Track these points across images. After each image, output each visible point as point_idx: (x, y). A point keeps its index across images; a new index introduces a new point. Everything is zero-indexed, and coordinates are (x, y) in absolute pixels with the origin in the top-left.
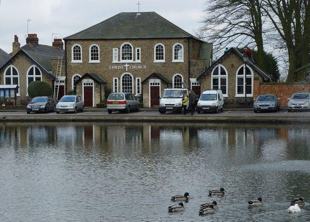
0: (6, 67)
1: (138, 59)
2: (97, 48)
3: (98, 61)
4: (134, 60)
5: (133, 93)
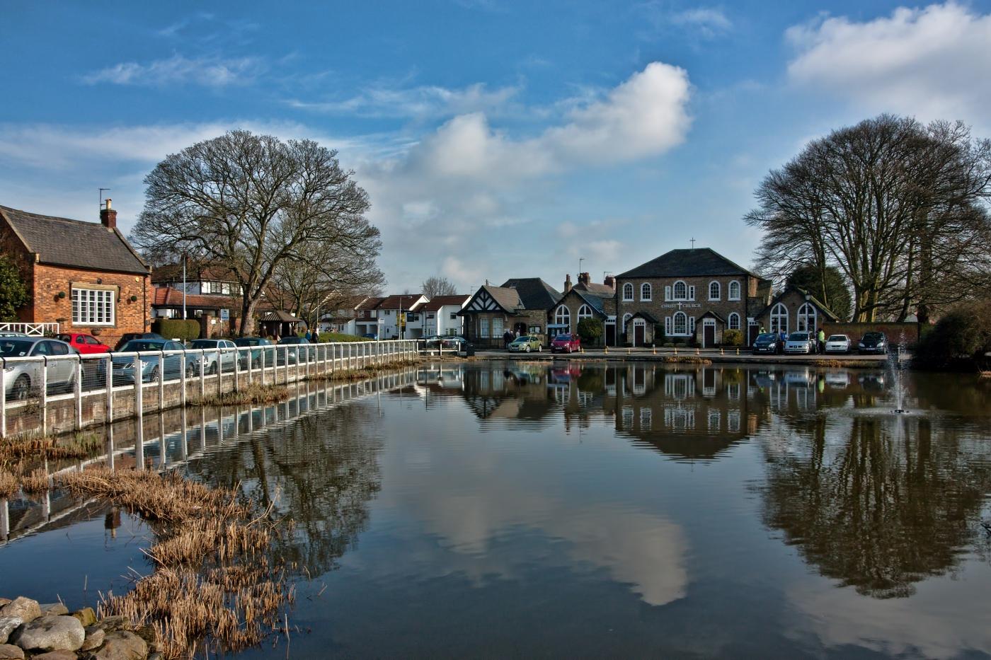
4: (688, 298)
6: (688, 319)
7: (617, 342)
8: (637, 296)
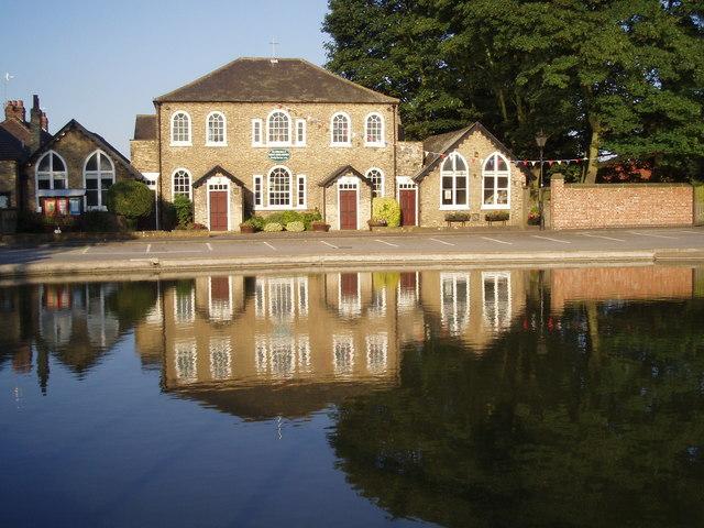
0: (38, 157)
1: (300, 138)
2: (221, 118)
3: (224, 144)
4: (293, 142)
5: (191, 198)
6: (295, 178)
7: (160, 220)
8: (199, 136)
